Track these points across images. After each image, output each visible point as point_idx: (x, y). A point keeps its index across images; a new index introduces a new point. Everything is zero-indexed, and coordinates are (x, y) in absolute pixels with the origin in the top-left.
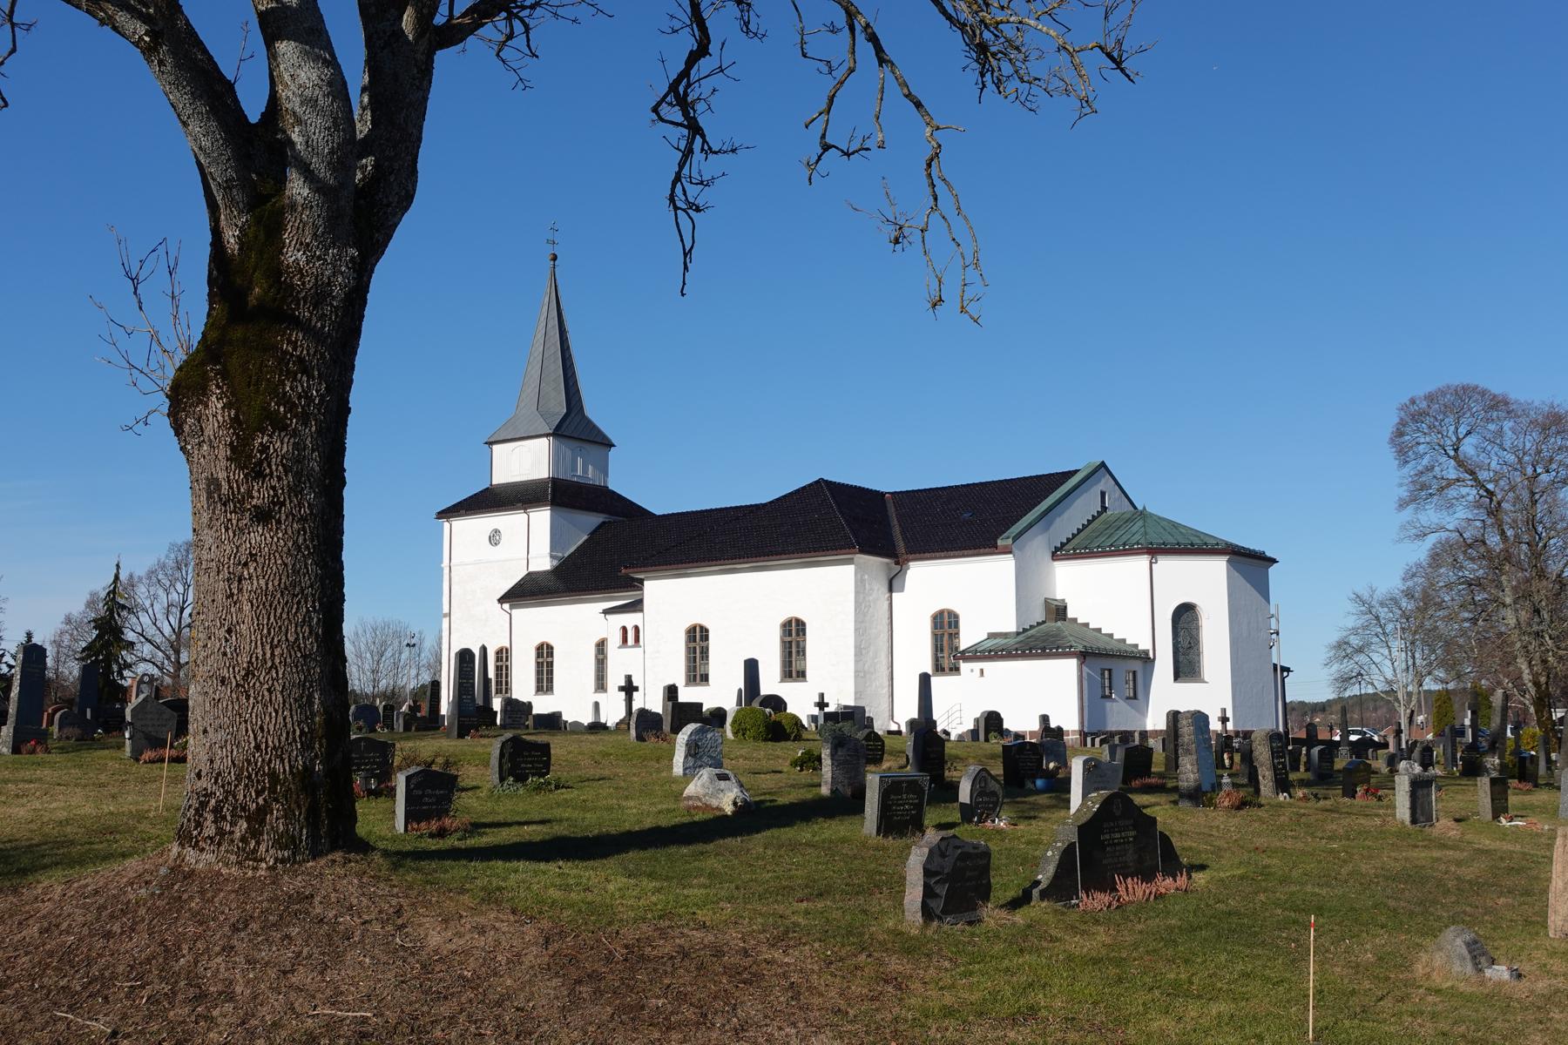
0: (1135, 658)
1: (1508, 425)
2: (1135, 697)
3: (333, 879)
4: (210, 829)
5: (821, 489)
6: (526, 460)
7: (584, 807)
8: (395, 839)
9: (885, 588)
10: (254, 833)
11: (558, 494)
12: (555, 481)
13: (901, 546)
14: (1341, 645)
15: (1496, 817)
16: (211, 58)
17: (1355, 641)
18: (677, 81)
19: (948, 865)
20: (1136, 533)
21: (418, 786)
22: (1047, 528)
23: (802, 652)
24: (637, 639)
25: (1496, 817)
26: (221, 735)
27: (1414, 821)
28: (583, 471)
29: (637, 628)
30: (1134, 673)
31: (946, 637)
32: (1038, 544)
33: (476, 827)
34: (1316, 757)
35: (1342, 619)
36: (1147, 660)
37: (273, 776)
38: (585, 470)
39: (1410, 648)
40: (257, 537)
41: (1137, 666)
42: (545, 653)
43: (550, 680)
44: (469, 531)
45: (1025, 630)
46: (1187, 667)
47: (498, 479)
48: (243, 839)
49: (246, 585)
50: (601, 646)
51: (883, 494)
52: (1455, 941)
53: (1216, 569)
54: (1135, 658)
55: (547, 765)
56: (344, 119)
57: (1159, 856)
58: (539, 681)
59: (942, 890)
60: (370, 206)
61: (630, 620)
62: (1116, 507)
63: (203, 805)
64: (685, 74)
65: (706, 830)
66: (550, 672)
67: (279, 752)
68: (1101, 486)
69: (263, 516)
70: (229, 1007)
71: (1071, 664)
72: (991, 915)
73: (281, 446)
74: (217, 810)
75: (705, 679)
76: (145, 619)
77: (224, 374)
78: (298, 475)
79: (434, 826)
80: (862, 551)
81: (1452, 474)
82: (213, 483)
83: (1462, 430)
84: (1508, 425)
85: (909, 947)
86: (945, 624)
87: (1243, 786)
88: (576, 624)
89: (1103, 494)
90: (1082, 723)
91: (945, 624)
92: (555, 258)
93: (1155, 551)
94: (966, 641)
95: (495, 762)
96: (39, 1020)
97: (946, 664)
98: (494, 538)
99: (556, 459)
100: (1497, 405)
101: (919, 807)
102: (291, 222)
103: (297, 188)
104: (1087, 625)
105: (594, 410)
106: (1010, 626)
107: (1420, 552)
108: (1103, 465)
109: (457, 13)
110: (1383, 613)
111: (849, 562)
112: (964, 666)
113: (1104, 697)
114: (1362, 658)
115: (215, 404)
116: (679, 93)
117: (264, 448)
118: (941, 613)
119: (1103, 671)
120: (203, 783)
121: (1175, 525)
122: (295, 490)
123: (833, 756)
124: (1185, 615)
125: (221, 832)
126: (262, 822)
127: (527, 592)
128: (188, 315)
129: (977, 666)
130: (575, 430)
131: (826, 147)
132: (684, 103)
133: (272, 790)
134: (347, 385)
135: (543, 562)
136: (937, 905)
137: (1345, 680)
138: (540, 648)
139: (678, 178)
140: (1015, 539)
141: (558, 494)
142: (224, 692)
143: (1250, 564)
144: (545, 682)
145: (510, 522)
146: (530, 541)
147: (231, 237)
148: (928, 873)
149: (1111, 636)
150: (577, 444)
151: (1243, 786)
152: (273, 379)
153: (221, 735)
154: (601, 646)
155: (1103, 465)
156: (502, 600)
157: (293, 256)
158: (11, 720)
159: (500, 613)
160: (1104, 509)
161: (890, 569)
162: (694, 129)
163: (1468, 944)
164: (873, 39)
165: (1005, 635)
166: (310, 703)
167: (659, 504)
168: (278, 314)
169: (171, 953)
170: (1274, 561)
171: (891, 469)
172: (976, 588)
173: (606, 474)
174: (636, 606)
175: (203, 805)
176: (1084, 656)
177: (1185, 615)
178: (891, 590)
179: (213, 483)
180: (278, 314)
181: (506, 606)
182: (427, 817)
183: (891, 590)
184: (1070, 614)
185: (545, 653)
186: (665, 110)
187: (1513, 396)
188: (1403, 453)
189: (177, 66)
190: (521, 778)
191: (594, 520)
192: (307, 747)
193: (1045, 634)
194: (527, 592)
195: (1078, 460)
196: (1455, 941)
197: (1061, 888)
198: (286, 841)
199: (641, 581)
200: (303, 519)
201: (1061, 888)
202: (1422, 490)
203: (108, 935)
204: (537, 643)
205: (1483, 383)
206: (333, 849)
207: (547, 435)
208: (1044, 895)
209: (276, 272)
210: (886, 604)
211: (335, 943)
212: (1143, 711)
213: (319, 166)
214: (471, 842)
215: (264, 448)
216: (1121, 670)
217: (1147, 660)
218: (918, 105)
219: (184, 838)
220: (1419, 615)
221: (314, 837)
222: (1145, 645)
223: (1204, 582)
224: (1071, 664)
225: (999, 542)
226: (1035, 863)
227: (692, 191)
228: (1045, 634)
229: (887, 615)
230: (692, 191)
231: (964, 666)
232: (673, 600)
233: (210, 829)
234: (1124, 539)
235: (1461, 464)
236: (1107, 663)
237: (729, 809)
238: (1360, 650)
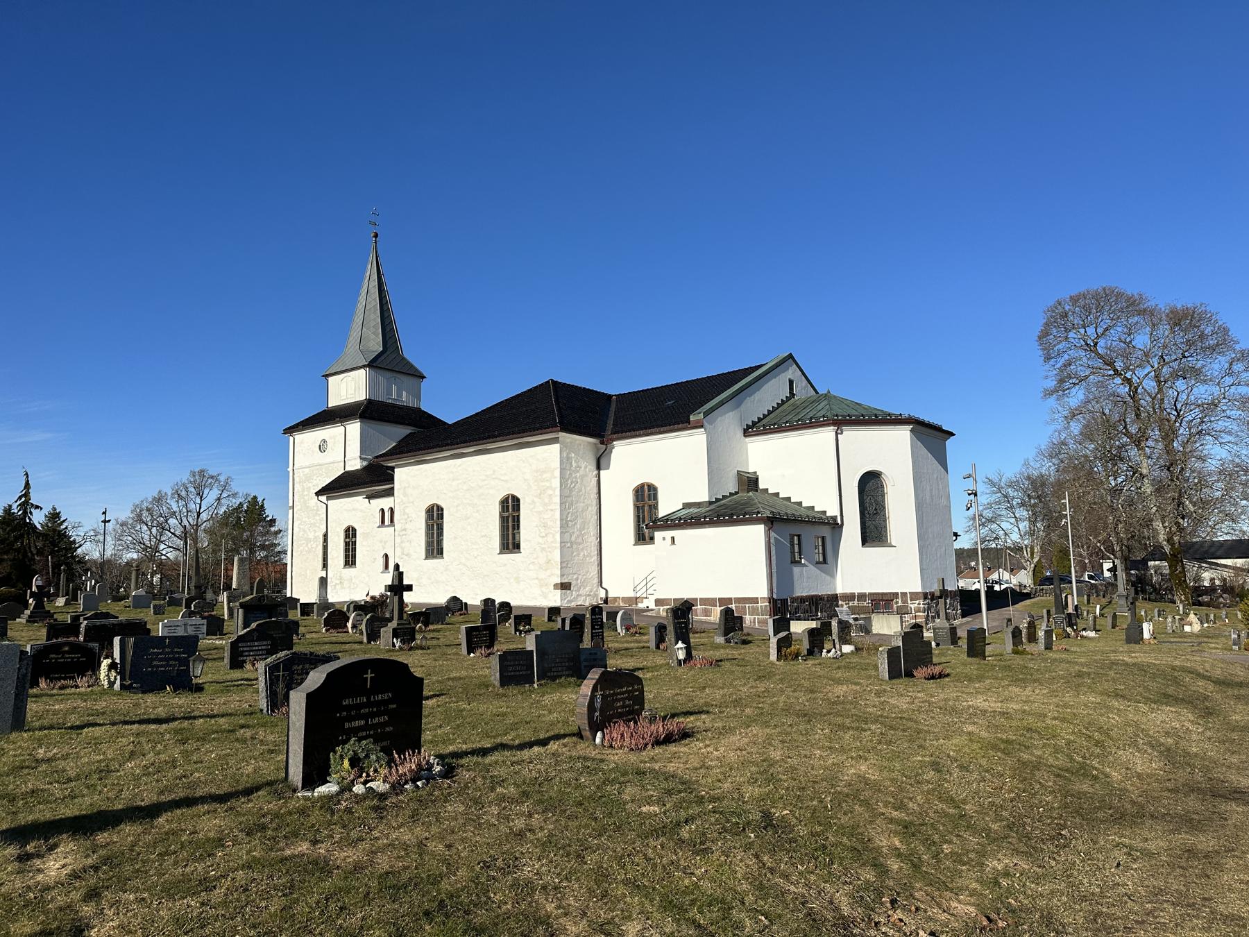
0: (823, 523)
2: (825, 562)
6: (349, 388)
9: (593, 466)
22: (738, 405)
23: (517, 526)
24: (392, 521)
28: (399, 394)
29: (392, 510)
30: (823, 538)
31: (646, 508)
32: (729, 421)
36: (835, 526)
38: (400, 395)
39: (1033, 520)
41: (826, 531)
43: (354, 556)
44: (306, 440)
45: (717, 500)
46: (874, 532)
47: (333, 403)
51: (610, 396)
54: (823, 523)
58: (347, 556)
61: (385, 503)
62: (802, 392)
66: (354, 550)
71: (760, 528)
80: (566, 429)
86: (645, 496)
89: (791, 382)
90: (771, 590)
91: (645, 496)
92: (376, 236)
94: (664, 509)
98: (322, 447)
99: (371, 384)
104: (777, 494)
105: (410, 352)
106: (704, 497)
108: (790, 356)
110: (1011, 493)
111: (556, 441)
112: (658, 535)
113: (794, 562)
118: (642, 486)
119: (792, 536)
124: (871, 484)
127: (341, 486)
130: (388, 361)
135: (355, 464)
140: (706, 414)
141: (368, 412)
143: (932, 437)
145: (333, 433)
146: (344, 447)
149: (800, 504)
150: (389, 374)
155: (790, 356)
156: (318, 494)
160: (792, 395)
161: (598, 449)
165: (698, 505)
167: (450, 419)
170: (952, 434)
171: (614, 379)
172: (675, 463)
173: (419, 399)
174: (390, 492)
176: (772, 522)
177: (871, 484)
178: (599, 468)
181: (323, 498)
183: (599, 468)
184: (762, 486)
193: (737, 503)
194: (341, 486)
199: (392, 469)
204: (344, 527)
207: (364, 367)
210: (594, 481)
212: (832, 574)
216: (810, 536)
222: (833, 511)
223: (890, 451)
224: (760, 528)
225: (692, 418)
228: (737, 503)
229: (595, 490)
231: (658, 535)
234: (811, 415)
238: (991, 521)
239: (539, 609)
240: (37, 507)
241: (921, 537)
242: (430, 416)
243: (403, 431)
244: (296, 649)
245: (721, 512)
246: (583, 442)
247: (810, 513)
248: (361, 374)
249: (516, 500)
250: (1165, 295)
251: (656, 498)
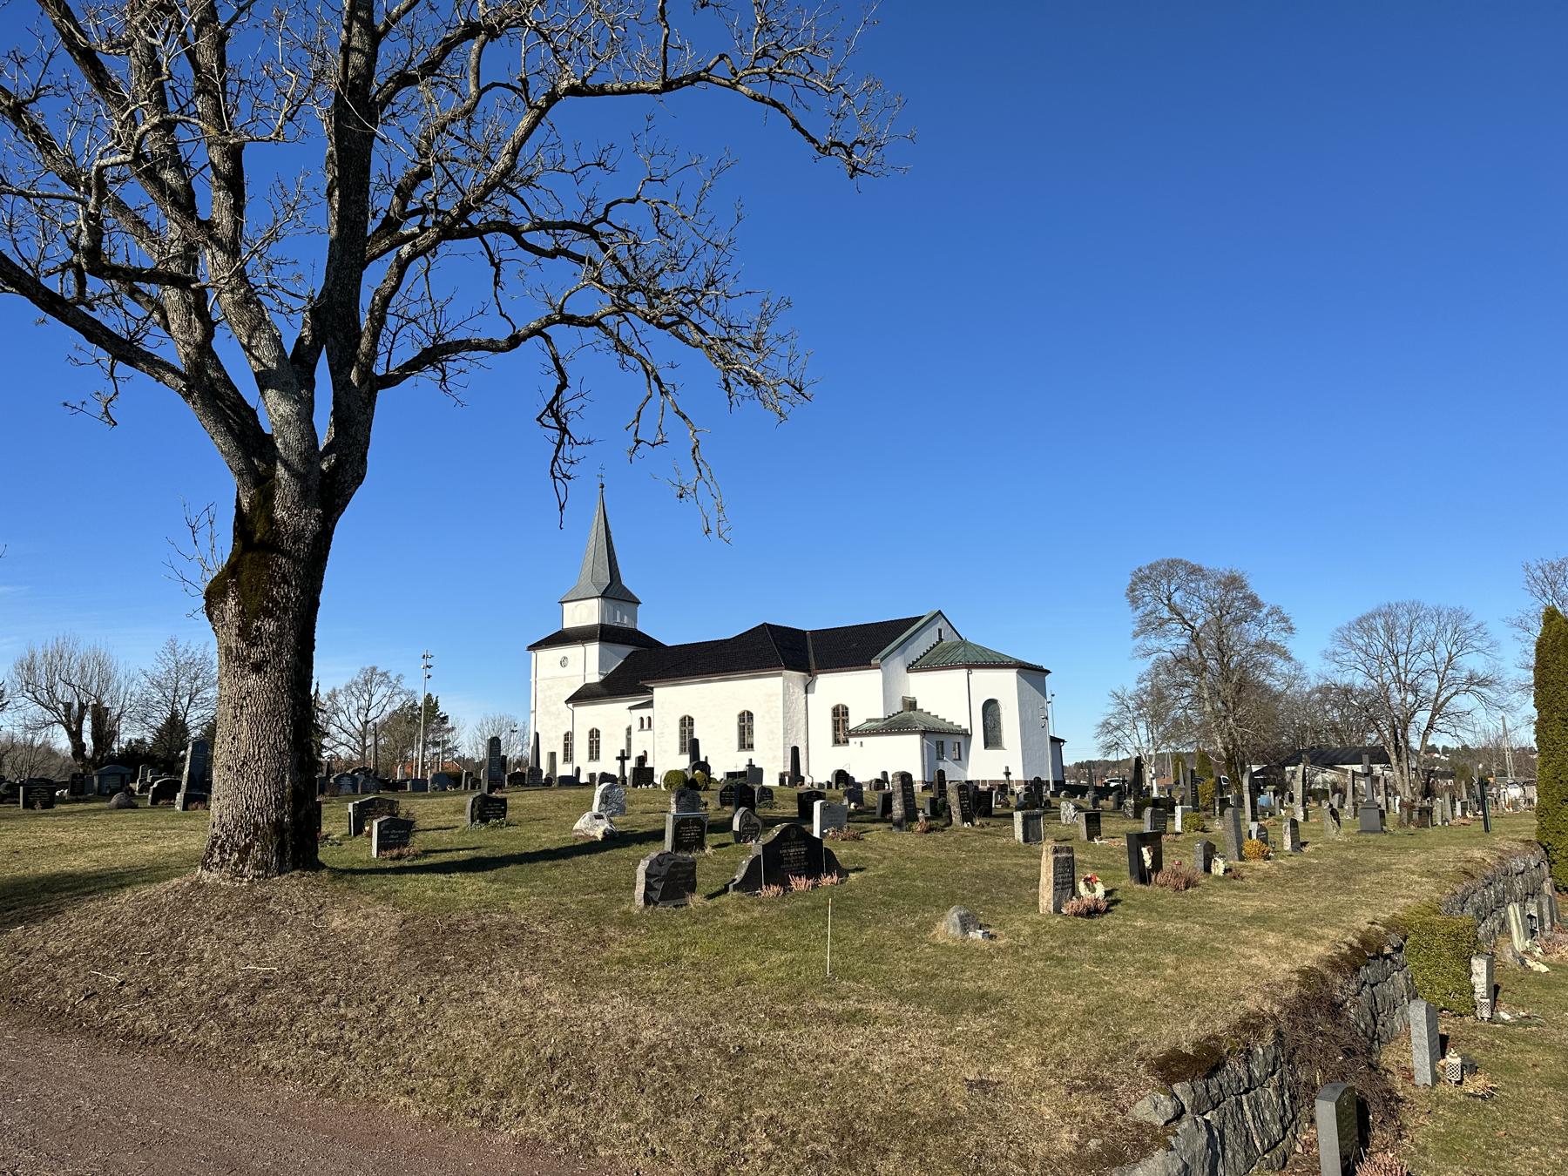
1: (1202, 584)
3: (291, 887)
4: (217, 859)
5: (767, 631)
6: (585, 613)
7: (516, 837)
8: (370, 860)
10: (242, 861)
11: (605, 634)
12: (602, 626)
13: (813, 667)
14: (1106, 724)
15: (1090, 838)
16: (240, 396)
17: (1114, 722)
18: (552, 403)
19: (664, 871)
20: (959, 655)
21: (386, 828)
23: (751, 732)
25: (1090, 838)
26: (227, 801)
27: (1026, 840)
32: (897, 664)
33: (426, 853)
34: (1106, 791)
35: (1106, 709)
36: (967, 735)
37: (256, 825)
40: (253, 680)
41: (960, 739)
42: (594, 735)
46: (992, 739)
47: (569, 624)
48: (235, 864)
49: (245, 711)
50: (629, 730)
52: (953, 915)
53: (1011, 675)
55: (504, 812)
56: (310, 434)
57: (817, 861)
58: (591, 753)
59: (660, 886)
60: (333, 481)
61: (645, 713)
62: (949, 638)
63: (214, 843)
64: (556, 398)
65: (591, 847)
67: (260, 811)
68: (939, 626)
69: (257, 668)
70: (196, 966)
72: (696, 900)
73: (270, 626)
74: (222, 846)
75: (751, 746)
76: (343, 717)
77: (236, 585)
78: (279, 644)
79: (395, 852)
81: (1166, 615)
82: (229, 649)
83: (1173, 588)
84: (1202, 584)
85: (628, 921)
86: (840, 714)
88: (613, 716)
91: (840, 714)
93: (970, 666)
94: (852, 724)
95: (468, 811)
96: (82, 976)
97: (842, 737)
98: (564, 662)
100: (1195, 571)
101: (702, 835)
102: (279, 494)
103: (281, 472)
107: (1146, 665)
109: (392, 368)
112: (851, 740)
114: (1119, 733)
115: (231, 603)
116: (553, 409)
117: (258, 629)
120: (217, 830)
121: (985, 650)
122: (277, 653)
123: (677, 802)
124: (990, 707)
125: (223, 860)
126: (248, 853)
127: (584, 696)
128: (223, 547)
129: (858, 740)
130: (615, 593)
131: (638, 442)
132: (556, 415)
133: (255, 834)
134: (317, 589)
135: (594, 678)
136: (656, 895)
137: (1109, 748)
138: (591, 732)
139: (555, 459)
141: (605, 634)
142: (230, 775)
143: (1033, 674)
144: (594, 754)
145: (574, 652)
146: (586, 663)
147: (245, 502)
148: (648, 875)
152: (272, 585)
153: (227, 801)
154: (629, 730)
157: (280, 514)
158: (183, 789)
159: (566, 710)
162: (564, 431)
163: (961, 917)
164: (657, 379)
165: (877, 720)
166: (283, 780)
167: (669, 639)
168: (271, 546)
169: (174, 933)
171: (810, 615)
172: (860, 691)
174: (649, 704)
175: (214, 843)
177: (990, 707)
179: (229, 649)
180: (271, 546)
182: (391, 847)
185: (594, 735)
186: (546, 419)
187: (1204, 566)
188: (1135, 602)
189: (204, 405)
190: (485, 820)
191: (628, 650)
192: (279, 807)
194: (584, 696)
195: (926, 611)
196: (953, 915)
197: (750, 883)
198: (263, 865)
200: (282, 671)
201: (750, 883)
202: (1151, 625)
203: (143, 924)
205: (1185, 559)
206: (294, 869)
208: (736, 888)
209: (271, 521)
211: (274, 923)
212: (965, 768)
213: (294, 459)
214: (416, 862)
215: (258, 629)
216: (949, 743)
218: (684, 417)
219: (206, 866)
220: (1154, 705)
221: (281, 862)
222: (966, 726)
223: (1003, 685)
226: (734, 872)
227: (565, 467)
230: (565, 467)
231: (851, 740)
232: (672, 700)
233: (217, 859)
235: (1172, 609)
236: (940, 738)
237: (600, 837)
238: (1118, 728)
243: (628, 650)
245: (893, 726)
246: (796, 676)
248: (595, 604)
249: (750, 715)
250: (1218, 562)
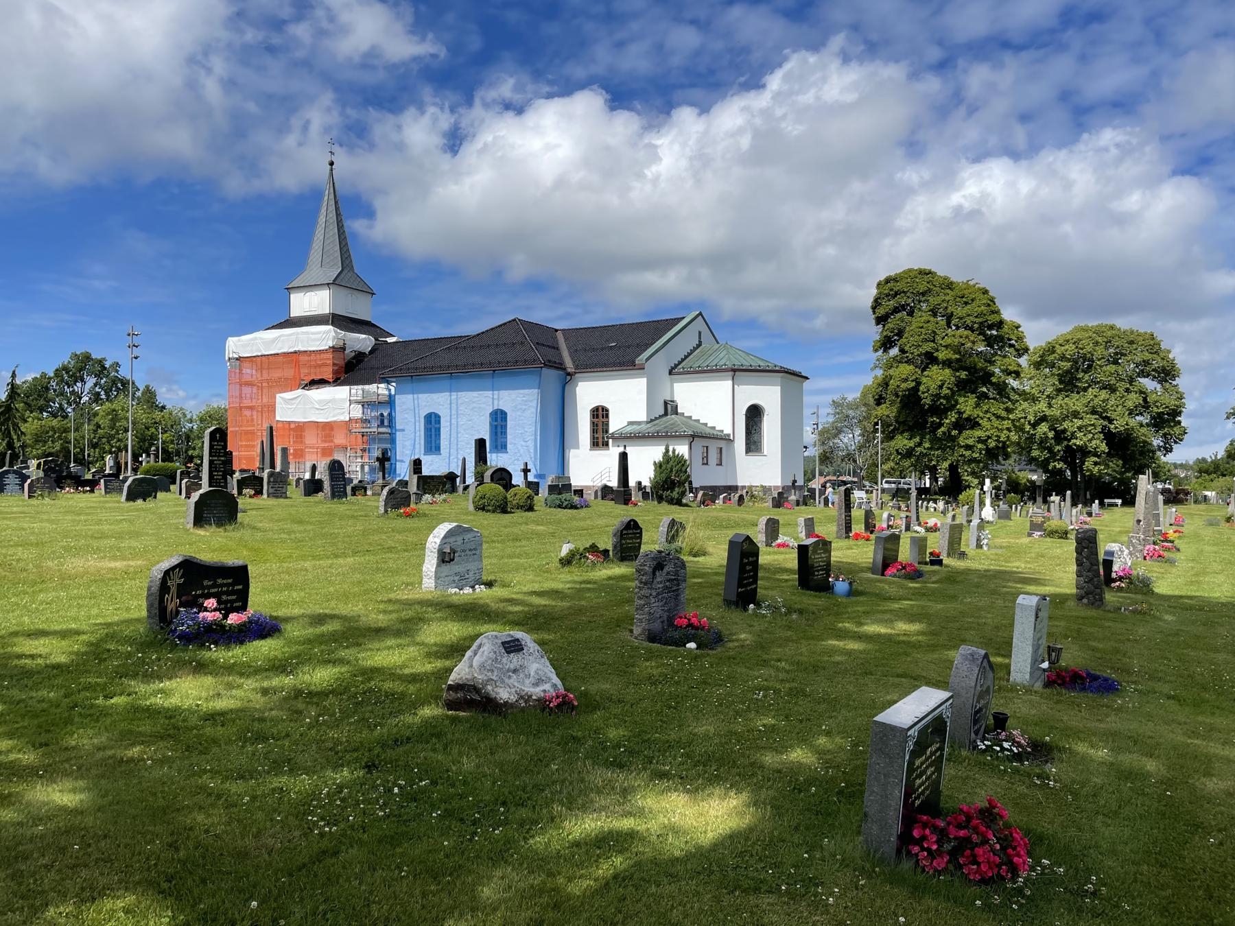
23: (504, 433)
28: (360, 308)
32: (661, 363)
36: (728, 440)
41: (722, 444)
46: (753, 444)
86: (600, 415)
87: (526, 477)
92: (332, 164)
99: (334, 300)
151: (526, 477)
165: (639, 423)
177: (754, 413)
184: (679, 411)
216: (713, 447)
217: (728, 440)
222: (728, 430)
223: (769, 396)
239: (588, 487)
240: (14, 375)
241: (747, 444)
242: (909, 693)
244: (251, 610)
247: (712, 432)
251: (607, 416)
